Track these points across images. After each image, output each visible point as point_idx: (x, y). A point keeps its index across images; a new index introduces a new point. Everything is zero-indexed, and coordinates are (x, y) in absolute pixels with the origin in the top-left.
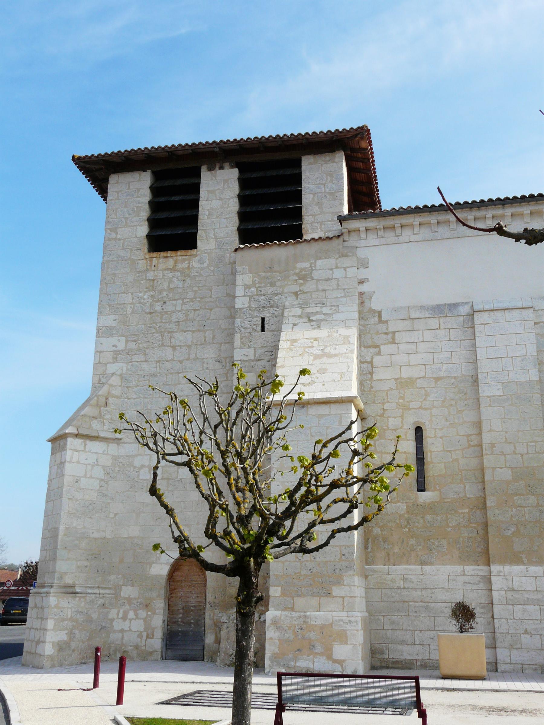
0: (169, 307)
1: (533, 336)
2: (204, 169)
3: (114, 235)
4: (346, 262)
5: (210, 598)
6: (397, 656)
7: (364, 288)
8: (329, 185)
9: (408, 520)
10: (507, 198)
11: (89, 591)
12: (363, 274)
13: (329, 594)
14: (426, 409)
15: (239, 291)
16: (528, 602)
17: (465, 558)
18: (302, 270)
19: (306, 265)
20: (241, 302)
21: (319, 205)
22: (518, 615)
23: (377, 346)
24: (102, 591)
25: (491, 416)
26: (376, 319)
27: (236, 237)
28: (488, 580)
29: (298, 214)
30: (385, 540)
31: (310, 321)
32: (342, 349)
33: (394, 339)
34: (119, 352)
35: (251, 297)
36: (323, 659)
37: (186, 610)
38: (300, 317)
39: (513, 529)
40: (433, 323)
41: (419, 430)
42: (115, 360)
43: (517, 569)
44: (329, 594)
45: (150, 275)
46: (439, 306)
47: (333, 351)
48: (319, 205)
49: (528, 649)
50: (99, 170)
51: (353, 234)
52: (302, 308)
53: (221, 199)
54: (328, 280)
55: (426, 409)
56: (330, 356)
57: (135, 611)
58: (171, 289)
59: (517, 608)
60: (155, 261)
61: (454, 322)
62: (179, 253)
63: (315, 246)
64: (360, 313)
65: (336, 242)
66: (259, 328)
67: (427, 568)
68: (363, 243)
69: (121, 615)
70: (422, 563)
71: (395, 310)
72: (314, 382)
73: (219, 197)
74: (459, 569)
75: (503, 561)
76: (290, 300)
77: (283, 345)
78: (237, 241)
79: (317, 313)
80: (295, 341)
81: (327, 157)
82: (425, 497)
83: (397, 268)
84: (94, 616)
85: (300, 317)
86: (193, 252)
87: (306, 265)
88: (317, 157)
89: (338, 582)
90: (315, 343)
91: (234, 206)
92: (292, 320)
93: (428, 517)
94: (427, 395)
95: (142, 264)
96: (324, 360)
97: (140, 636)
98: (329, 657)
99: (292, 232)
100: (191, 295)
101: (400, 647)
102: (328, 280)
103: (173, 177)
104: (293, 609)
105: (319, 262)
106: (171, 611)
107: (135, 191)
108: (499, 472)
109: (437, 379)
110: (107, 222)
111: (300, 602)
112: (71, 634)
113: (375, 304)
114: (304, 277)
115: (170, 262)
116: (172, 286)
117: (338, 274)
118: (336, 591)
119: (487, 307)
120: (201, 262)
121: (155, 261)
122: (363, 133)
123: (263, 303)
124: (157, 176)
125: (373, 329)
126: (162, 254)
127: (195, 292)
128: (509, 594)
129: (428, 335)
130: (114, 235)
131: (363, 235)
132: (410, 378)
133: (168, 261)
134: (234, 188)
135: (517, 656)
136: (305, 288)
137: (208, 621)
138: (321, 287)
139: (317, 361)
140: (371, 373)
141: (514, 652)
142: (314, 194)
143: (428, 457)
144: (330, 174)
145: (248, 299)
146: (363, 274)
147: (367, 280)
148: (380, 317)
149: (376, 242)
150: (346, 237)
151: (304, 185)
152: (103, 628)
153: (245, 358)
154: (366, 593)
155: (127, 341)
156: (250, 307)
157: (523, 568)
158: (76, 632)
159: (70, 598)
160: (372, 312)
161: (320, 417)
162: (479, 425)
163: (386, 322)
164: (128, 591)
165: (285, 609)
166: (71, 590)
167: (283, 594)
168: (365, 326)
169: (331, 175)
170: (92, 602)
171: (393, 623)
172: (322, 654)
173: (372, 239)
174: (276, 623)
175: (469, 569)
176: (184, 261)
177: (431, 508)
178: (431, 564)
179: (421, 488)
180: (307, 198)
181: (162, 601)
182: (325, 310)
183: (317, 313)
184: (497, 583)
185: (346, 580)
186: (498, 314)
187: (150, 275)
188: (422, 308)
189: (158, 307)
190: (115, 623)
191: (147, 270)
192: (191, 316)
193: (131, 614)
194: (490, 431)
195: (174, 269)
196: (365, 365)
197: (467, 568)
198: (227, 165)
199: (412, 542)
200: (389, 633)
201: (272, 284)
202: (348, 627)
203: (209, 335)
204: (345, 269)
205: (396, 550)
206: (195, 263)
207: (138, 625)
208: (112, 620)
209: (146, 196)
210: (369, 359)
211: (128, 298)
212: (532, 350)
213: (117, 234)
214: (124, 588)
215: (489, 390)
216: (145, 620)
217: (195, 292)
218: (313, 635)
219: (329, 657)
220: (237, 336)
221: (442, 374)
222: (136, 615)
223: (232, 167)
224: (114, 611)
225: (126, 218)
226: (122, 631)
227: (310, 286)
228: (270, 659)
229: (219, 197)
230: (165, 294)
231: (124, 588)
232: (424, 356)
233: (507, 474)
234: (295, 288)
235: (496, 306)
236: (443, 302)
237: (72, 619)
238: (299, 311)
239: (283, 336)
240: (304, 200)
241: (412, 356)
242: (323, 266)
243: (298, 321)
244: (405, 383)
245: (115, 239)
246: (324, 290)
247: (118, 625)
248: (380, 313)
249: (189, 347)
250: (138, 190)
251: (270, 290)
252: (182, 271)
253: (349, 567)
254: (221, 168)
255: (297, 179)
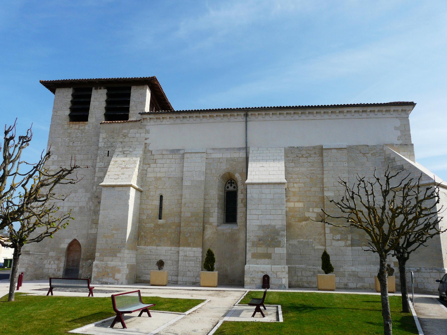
0: (75, 144)
1: (204, 164)
2: (93, 88)
3: (56, 114)
4: (141, 131)
5: (82, 257)
6: (145, 279)
7: (147, 141)
8: (141, 99)
9: (154, 230)
10: (201, 110)
11: (36, 253)
12: (147, 136)
13: (116, 256)
14: (164, 189)
15: (101, 140)
16: (191, 260)
17: (172, 244)
18: (125, 133)
19: (126, 131)
20: (101, 144)
21: (136, 106)
22: (187, 265)
23: (149, 164)
24: (41, 253)
25: (186, 193)
26: (150, 154)
27: (103, 118)
28: (178, 252)
29: (128, 110)
30: (145, 237)
31: (124, 154)
32: (132, 166)
33: (155, 162)
34: (55, 161)
35: (105, 143)
36: (112, 279)
37: (73, 261)
38: (121, 152)
39: (189, 234)
40: (170, 156)
41: (161, 197)
42: (53, 164)
43: (188, 248)
44: (116, 256)
45: (69, 131)
46: (173, 150)
47: (129, 166)
48: (136, 106)
49: (189, 277)
50: (53, 86)
51: (145, 120)
52: (122, 148)
53: (99, 102)
54: (134, 137)
55: (164, 189)
56: (127, 168)
57: (54, 261)
58: (77, 137)
59: (187, 262)
60: (71, 125)
61: (178, 156)
62: (81, 123)
63: (130, 124)
64: (144, 151)
65: (138, 123)
66: (107, 155)
67: (159, 248)
68: (148, 124)
69: (48, 263)
70: (157, 246)
71: (157, 150)
72: (119, 178)
73: (98, 101)
74: (169, 248)
75: (184, 246)
76: (119, 145)
77: (112, 163)
78: (104, 119)
79: (127, 151)
80: (116, 161)
81: (141, 87)
82: (161, 221)
83: (162, 134)
84: (37, 263)
85: (121, 152)
86: (86, 122)
87: (126, 131)
88: (138, 87)
89: (119, 252)
90: (123, 163)
91: (104, 105)
92: (117, 153)
93: (161, 229)
94: (165, 184)
95: (66, 126)
96: (125, 169)
97: (55, 270)
98: (114, 278)
99: (125, 118)
100: (84, 140)
101: (146, 276)
102: (134, 137)
103: (79, 93)
104: (103, 261)
105: (131, 130)
106: (67, 261)
107: (67, 95)
108: (186, 213)
109: (169, 178)
110: (54, 108)
111: (106, 258)
112: (27, 269)
113: (150, 148)
114: (125, 136)
115: (77, 126)
116: (77, 136)
117: (138, 135)
118: (118, 255)
119: (189, 151)
120: (89, 127)
121: (71, 125)
122: (19, 137)
123: (109, 145)
124: (76, 90)
125: (148, 158)
126: (74, 123)
127: (86, 139)
128: (185, 258)
129: (168, 161)
130: (56, 114)
131: (149, 121)
132: (160, 177)
133: (77, 126)
134: (105, 97)
135: (185, 279)
136: (125, 140)
137: (81, 266)
138: (131, 140)
139: (122, 170)
140: (146, 174)
141: (184, 278)
142: (135, 102)
143: (163, 207)
144: (141, 94)
145: (103, 143)
146: (147, 136)
147: (148, 138)
148: (152, 153)
149: (153, 124)
150: (142, 121)
151: (131, 98)
152: (41, 267)
153: (100, 166)
154: (137, 256)
155: (58, 157)
156: (104, 147)
157: (190, 248)
158: (29, 268)
159: (27, 256)
160: (149, 151)
161: (119, 191)
162: (181, 196)
163: (154, 155)
164: (52, 254)
165: (101, 261)
166: (28, 253)
167: (100, 256)
168: (146, 156)
169: (142, 95)
170: (37, 257)
171: (145, 267)
172: (111, 277)
173: (152, 122)
174: (96, 266)
175: (173, 248)
176: (82, 126)
177: (162, 226)
178: (160, 246)
179: (160, 218)
180: (132, 104)
181: (64, 258)
182: (131, 150)
183: (127, 151)
184: (181, 253)
185: (122, 251)
186: (193, 154)
187: (69, 131)
188: (167, 150)
189: (71, 144)
190: (46, 266)
191: (68, 129)
192: (84, 148)
193: (52, 262)
194: (185, 198)
195: (78, 129)
196: (144, 171)
197: (172, 248)
198: (102, 88)
199: (154, 238)
200: (143, 271)
201: (113, 138)
202: (121, 268)
203: (90, 156)
204: (140, 134)
205: (149, 241)
206: (87, 127)
207: (54, 266)
208: (45, 264)
209: (70, 98)
210: (146, 169)
211: (59, 140)
212: (204, 169)
213: (57, 113)
214: (50, 253)
215: (186, 183)
216: (57, 264)
217: (86, 139)
218: (109, 270)
219: (114, 278)
220: (98, 158)
221: (171, 176)
222: (54, 262)
223: (104, 89)
224: (46, 261)
225: (61, 107)
226: (48, 268)
227: (127, 140)
228: (94, 279)
229: (98, 101)
230: (74, 139)
231: (50, 253)
232: (164, 169)
233: (189, 214)
234: (121, 140)
235: (193, 151)
236: (175, 148)
237: (27, 264)
238: (121, 149)
239: (113, 159)
240: (130, 104)
241: (161, 169)
242: (133, 132)
243: (120, 153)
244: (157, 179)
245: (56, 115)
246: (132, 142)
247: (47, 266)
248: (152, 151)
249: (82, 160)
250: (67, 96)
251: (112, 140)
252: (81, 130)
253: (124, 247)
254: (100, 89)
255: (129, 95)
